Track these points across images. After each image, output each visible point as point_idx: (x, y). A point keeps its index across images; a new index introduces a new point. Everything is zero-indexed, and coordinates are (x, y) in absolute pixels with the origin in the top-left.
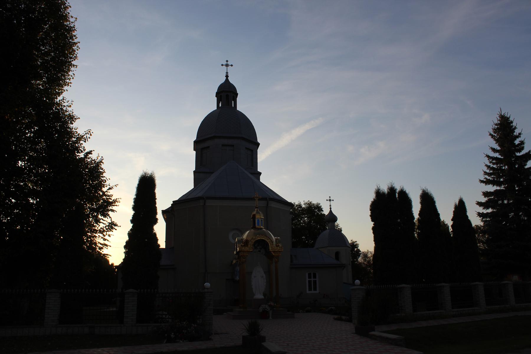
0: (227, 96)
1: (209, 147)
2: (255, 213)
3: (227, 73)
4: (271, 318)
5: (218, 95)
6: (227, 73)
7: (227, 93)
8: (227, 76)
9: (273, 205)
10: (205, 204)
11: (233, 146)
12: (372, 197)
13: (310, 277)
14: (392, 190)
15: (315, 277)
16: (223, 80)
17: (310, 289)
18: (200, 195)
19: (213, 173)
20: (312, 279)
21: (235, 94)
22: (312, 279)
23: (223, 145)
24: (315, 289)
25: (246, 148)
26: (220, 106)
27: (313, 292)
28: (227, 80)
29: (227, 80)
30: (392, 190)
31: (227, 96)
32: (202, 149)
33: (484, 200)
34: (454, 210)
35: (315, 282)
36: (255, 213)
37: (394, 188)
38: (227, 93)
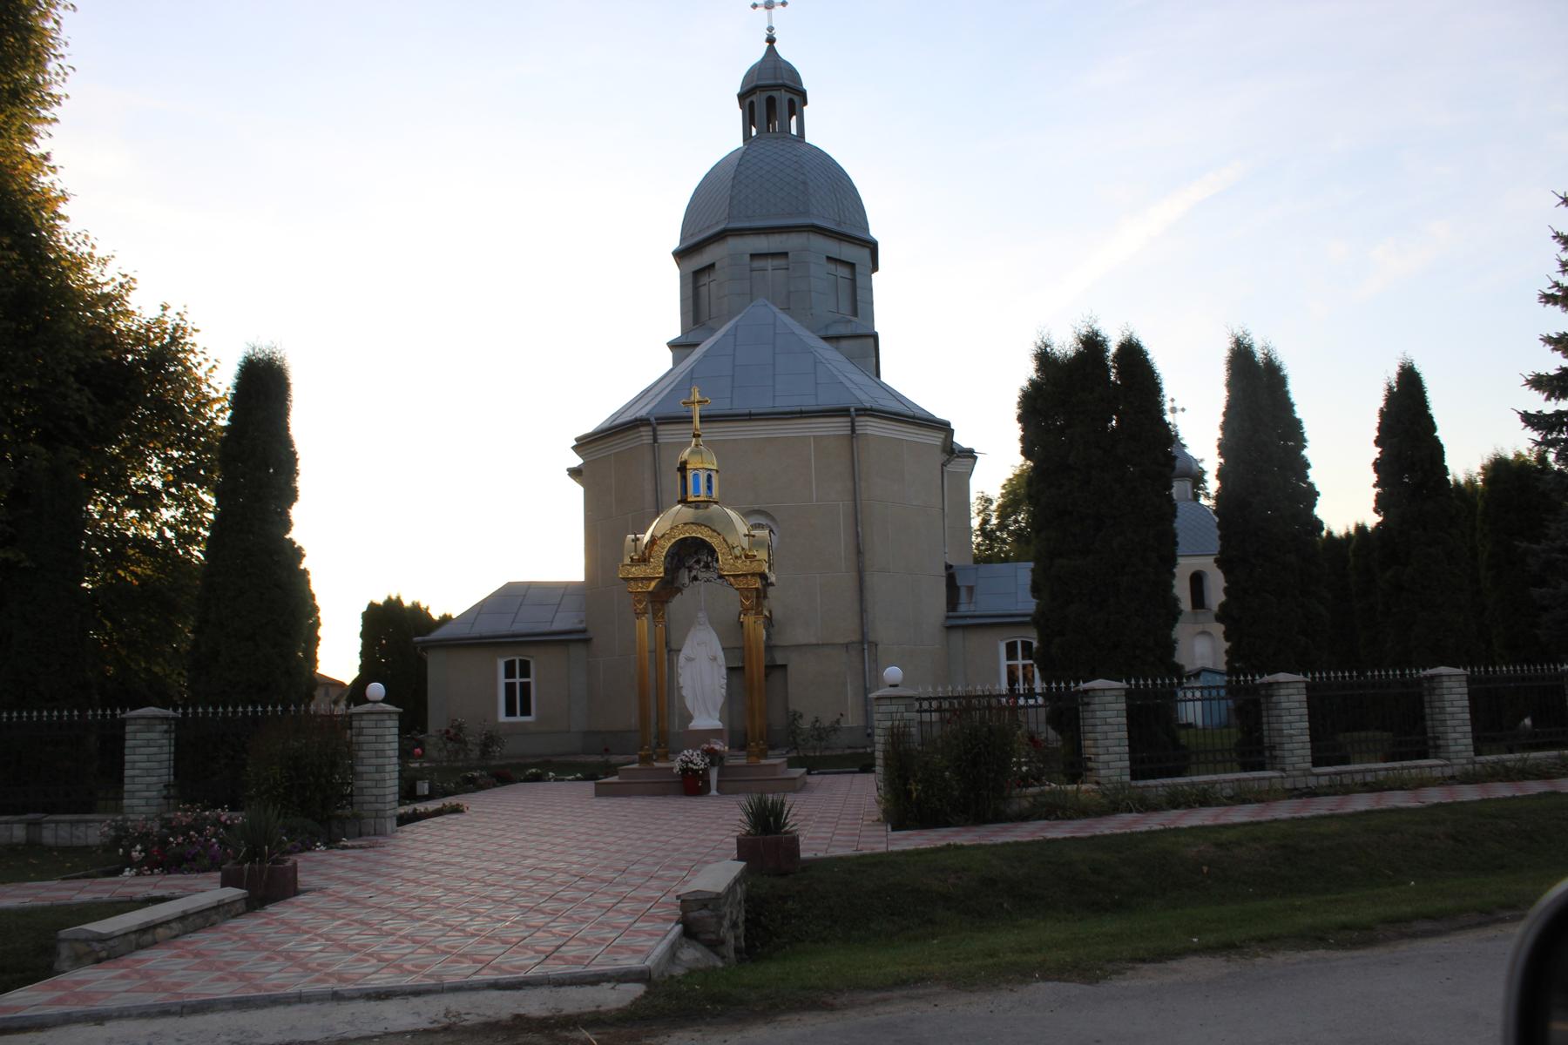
0: (771, 102)
1: (712, 266)
2: (686, 454)
3: (771, 29)
4: (714, 792)
5: (746, 97)
6: (771, 29)
7: (772, 96)
8: (771, 40)
9: (872, 428)
10: (655, 440)
11: (785, 254)
12: (1027, 371)
13: (510, 672)
14: (1092, 344)
15: (525, 672)
16: (758, 52)
17: (510, 711)
18: (643, 413)
19: (697, 345)
20: (518, 680)
21: (797, 98)
22: (518, 680)
23: (753, 256)
24: (526, 711)
25: (829, 258)
26: (754, 132)
27: (519, 719)
28: (771, 50)
29: (771, 50)
30: (1092, 344)
31: (771, 102)
32: (697, 274)
33: (1552, 363)
34: (1382, 404)
35: (526, 688)
36: (686, 454)
37: (1096, 334)
38: (772, 96)
